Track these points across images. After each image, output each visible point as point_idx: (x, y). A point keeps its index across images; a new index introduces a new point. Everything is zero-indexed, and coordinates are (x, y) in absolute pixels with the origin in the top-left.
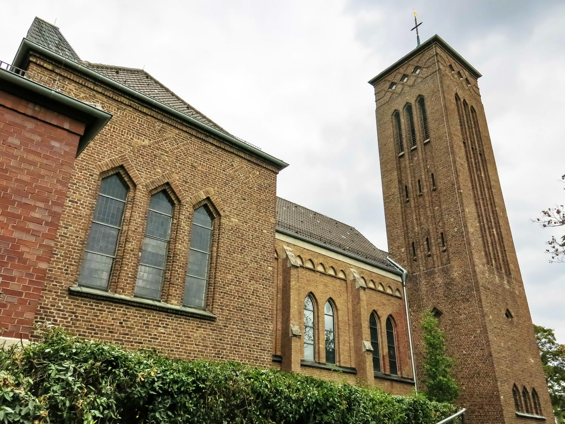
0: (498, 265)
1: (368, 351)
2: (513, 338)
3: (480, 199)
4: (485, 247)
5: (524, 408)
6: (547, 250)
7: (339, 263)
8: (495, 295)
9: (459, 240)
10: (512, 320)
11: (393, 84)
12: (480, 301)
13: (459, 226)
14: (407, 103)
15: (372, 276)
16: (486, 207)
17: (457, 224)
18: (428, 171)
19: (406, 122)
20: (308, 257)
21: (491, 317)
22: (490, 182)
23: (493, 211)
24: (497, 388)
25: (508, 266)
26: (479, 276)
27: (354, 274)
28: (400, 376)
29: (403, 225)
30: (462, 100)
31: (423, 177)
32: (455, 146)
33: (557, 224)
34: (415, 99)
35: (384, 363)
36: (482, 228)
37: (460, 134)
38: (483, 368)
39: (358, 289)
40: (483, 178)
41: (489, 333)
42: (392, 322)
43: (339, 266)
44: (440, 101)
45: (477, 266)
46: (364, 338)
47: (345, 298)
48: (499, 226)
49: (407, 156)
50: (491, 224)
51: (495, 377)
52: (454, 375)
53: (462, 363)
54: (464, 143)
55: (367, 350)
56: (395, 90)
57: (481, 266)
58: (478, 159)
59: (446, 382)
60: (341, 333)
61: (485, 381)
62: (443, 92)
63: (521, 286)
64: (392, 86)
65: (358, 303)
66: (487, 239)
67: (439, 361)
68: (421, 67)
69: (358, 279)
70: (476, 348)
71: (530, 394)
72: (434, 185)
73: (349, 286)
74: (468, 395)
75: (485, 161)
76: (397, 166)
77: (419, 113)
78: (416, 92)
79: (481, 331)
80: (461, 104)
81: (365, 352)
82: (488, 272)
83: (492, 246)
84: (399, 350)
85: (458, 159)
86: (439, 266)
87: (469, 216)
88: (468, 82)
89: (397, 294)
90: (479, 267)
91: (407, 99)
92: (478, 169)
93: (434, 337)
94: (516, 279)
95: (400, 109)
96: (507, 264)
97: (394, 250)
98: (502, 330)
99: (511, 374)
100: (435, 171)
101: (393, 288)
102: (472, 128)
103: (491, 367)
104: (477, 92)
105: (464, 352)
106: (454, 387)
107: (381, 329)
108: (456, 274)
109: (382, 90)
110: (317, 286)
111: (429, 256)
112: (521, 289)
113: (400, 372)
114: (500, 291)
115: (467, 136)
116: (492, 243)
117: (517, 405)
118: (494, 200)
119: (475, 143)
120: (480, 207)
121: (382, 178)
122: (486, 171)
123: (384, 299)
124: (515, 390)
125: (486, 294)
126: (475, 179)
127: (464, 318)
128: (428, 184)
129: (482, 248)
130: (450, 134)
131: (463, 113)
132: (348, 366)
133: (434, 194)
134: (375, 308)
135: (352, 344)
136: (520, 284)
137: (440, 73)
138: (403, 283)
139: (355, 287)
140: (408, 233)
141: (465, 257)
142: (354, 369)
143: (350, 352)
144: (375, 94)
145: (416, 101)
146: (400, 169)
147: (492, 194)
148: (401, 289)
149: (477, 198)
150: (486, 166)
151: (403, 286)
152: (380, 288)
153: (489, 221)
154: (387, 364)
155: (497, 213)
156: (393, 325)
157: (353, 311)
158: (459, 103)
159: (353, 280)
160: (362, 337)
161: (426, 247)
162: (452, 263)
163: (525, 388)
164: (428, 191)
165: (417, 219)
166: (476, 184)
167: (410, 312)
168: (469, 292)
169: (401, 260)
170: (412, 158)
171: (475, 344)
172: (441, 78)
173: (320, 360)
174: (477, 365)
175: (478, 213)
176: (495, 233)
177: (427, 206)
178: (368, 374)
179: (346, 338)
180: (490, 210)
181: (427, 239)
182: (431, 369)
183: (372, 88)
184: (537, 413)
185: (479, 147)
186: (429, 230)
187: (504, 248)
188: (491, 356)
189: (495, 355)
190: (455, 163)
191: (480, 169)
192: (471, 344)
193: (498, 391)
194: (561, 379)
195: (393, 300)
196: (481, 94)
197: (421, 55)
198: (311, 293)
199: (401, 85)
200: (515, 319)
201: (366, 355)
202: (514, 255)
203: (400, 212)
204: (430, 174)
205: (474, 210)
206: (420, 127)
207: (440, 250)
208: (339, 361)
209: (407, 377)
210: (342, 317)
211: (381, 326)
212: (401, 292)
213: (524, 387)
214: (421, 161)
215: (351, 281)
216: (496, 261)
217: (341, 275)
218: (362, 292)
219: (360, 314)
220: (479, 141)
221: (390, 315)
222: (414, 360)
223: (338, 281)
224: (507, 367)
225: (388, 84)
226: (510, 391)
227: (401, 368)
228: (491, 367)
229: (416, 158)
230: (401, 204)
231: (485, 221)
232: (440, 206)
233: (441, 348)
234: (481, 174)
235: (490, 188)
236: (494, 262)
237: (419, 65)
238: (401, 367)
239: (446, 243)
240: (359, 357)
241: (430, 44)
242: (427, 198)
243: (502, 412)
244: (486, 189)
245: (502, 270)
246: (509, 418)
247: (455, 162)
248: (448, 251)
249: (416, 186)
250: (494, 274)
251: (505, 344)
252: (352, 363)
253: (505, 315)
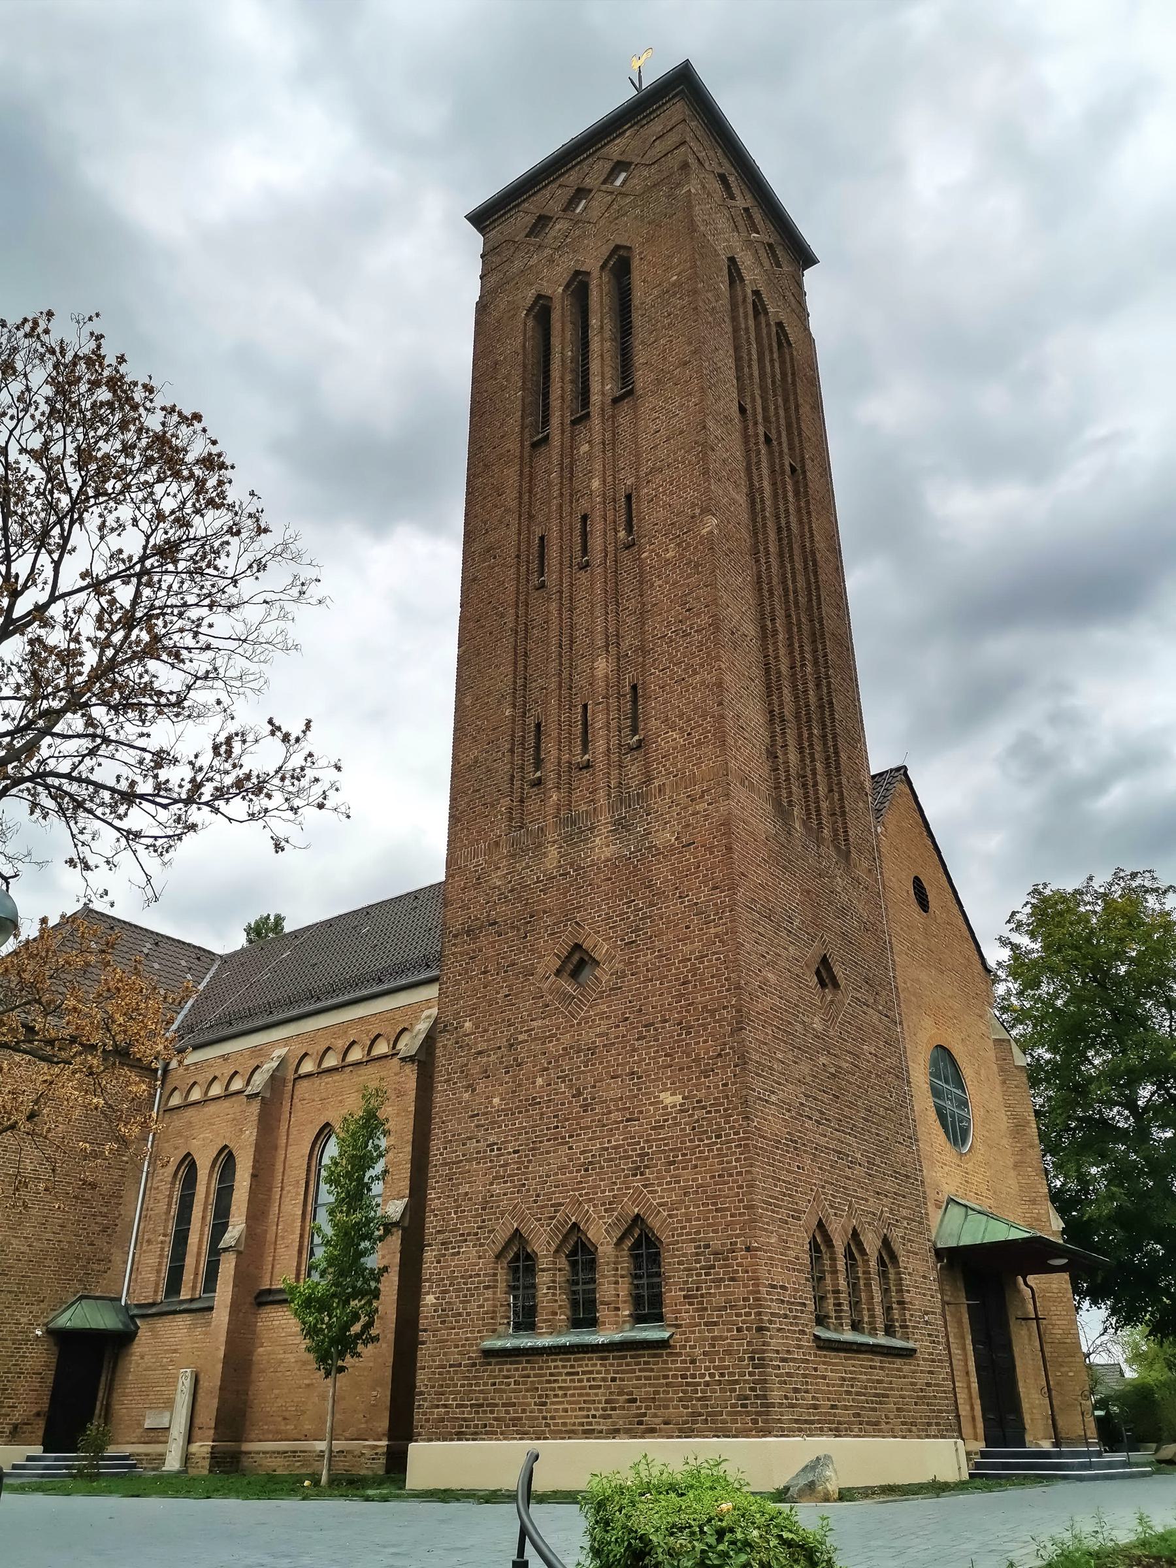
124: (820, 1241)
145: (603, 267)
183: (475, 241)
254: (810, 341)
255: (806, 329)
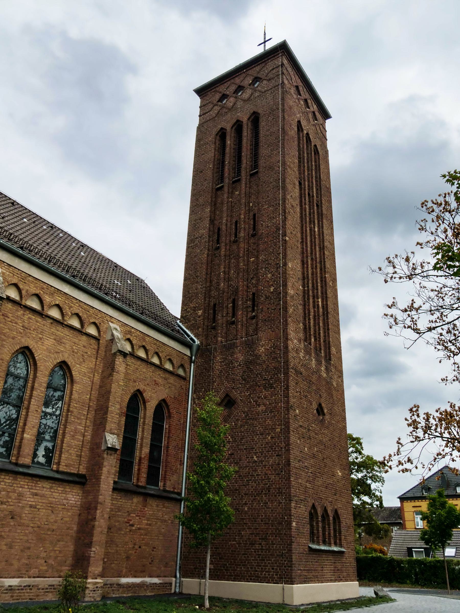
0: (318, 345)
1: (113, 449)
2: (321, 442)
3: (309, 257)
4: (305, 319)
5: (321, 538)
6: (385, 314)
7: (92, 311)
8: (307, 382)
9: (274, 304)
10: (323, 418)
11: (224, 96)
12: (287, 388)
13: (277, 284)
14: (238, 121)
15: (144, 340)
16: (314, 270)
17: (274, 281)
18: (249, 210)
19: (232, 145)
20: (33, 290)
21: (297, 411)
22: (323, 241)
23: (321, 278)
24: (290, 510)
25: (329, 349)
26: (291, 354)
27: (115, 332)
28: (162, 488)
29: (206, 279)
30: (305, 132)
31: (242, 216)
32: (287, 181)
33: (402, 280)
34: (248, 116)
35: (139, 470)
36: (305, 293)
37: (296, 169)
38: (275, 481)
39: (115, 354)
40: (317, 233)
41: (291, 433)
42: (166, 411)
43: (91, 316)
44: (277, 122)
45: (291, 340)
46: (108, 428)
47: (92, 366)
48: (326, 297)
49: (226, 189)
50: (317, 292)
51: (290, 495)
52: (237, 490)
53: (249, 473)
54: (300, 184)
55: (109, 448)
56: (225, 104)
57: (295, 341)
58: (313, 208)
59: (217, 502)
60: (71, 419)
61: (276, 501)
62: (283, 111)
63: (340, 377)
64: (224, 100)
65: (111, 375)
66: (309, 310)
67: (213, 470)
68: (261, 79)
69: (118, 338)
70: (272, 453)
71: (331, 518)
72: (254, 229)
73: (102, 348)
74: (249, 519)
75: (322, 215)
76: (212, 201)
77: (250, 135)
78: (249, 108)
79: (281, 430)
80: (303, 136)
81: (104, 451)
82: (305, 351)
83: (315, 320)
84: (167, 451)
85: (288, 197)
86: (242, 338)
87: (291, 273)
88: (315, 118)
89: (181, 372)
90: (293, 342)
91: (238, 116)
92: (312, 221)
93: (213, 433)
94: (335, 367)
95: (228, 127)
96: (328, 347)
97: (188, 312)
98: (309, 430)
99: (311, 491)
100: (259, 210)
101: (175, 362)
102: (312, 170)
103: (286, 481)
104: (324, 133)
105: (255, 458)
106: (227, 510)
107: (144, 418)
108: (262, 349)
109: (209, 102)
110: (41, 339)
111: (233, 323)
112: (340, 381)
113: (162, 483)
114: (314, 378)
115: (304, 176)
116: (315, 316)
117: (312, 533)
118: (324, 264)
119: (313, 189)
120: (307, 267)
121: (190, 215)
122: (321, 227)
123: (158, 376)
124: (313, 514)
125: (297, 380)
126: (306, 230)
127: (262, 410)
128: (247, 226)
129: (302, 319)
130: (284, 164)
131: (303, 147)
132: (72, 472)
133: (252, 241)
134: (141, 387)
135: (89, 438)
136: (340, 374)
137: (283, 88)
138: (191, 358)
139: (111, 351)
140: (210, 291)
141: (277, 327)
142: (83, 476)
143: (82, 450)
144: (200, 107)
145: (248, 119)
146: (215, 204)
147: (324, 256)
148: (187, 366)
149: (305, 255)
150: (322, 222)
151: (191, 362)
152: (155, 360)
153: (315, 288)
154: (144, 470)
155: (325, 281)
156: (166, 415)
157: (100, 387)
158: (301, 134)
159: (110, 340)
160: (105, 427)
161: (230, 310)
162: (261, 334)
163: (325, 510)
164: (245, 236)
165: (224, 272)
166: (306, 236)
167: (193, 399)
168: (274, 375)
169: (194, 327)
170: (232, 192)
171: (271, 447)
172: (283, 93)
173: (20, 458)
174: (268, 477)
175: (303, 274)
176: (320, 303)
177: (241, 255)
178: (101, 485)
179: (78, 427)
180: (319, 275)
181: (234, 300)
182: (198, 482)
183: (197, 100)
184: (336, 544)
185: (317, 197)
186: (237, 289)
187: (328, 325)
188: (289, 465)
189: (294, 463)
190: (285, 201)
191: (314, 222)
192: (265, 447)
193: (290, 515)
194: (363, 494)
195: (172, 379)
196: (327, 138)
197: (263, 65)
198: (27, 348)
199: (234, 98)
200: (327, 417)
201: (105, 456)
202: (338, 336)
203: (204, 261)
204: (251, 214)
205: (299, 267)
206: (249, 153)
207: (247, 316)
208: (58, 464)
209: (172, 490)
210: (79, 394)
211: (145, 414)
212: (187, 370)
213: (325, 508)
214: (243, 195)
215: (106, 341)
216: (315, 340)
217: (92, 331)
218: (119, 360)
219: (109, 392)
220: (318, 189)
221: (164, 400)
222: (187, 466)
223: (84, 338)
224: (307, 481)
225: (218, 96)
226: (307, 514)
227: (165, 477)
228: (286, 481)
229: (237, 193)
230: (208, 250)
231: (310, 285)
232: (257, 257)
233: (220, 451)
234: (314, 228)
235: (322, 248)
236: (313, 340)
237: (259, 76)
238: (165, 475)
239: (257, 307)
240: (95, 458)
241: (276, 52)
242: (242, 245)
243: (291, 545)
244: (317, 249)
245: (321, 353)
246: (299, 553)
247: (284, 200)
248: (257, 317)
249: (231, 228)
250: (310, 355)
251: (310, 448)
252: (81, 467)
253: (315, 411)
254: (327, 152)
255: (326, 147)
